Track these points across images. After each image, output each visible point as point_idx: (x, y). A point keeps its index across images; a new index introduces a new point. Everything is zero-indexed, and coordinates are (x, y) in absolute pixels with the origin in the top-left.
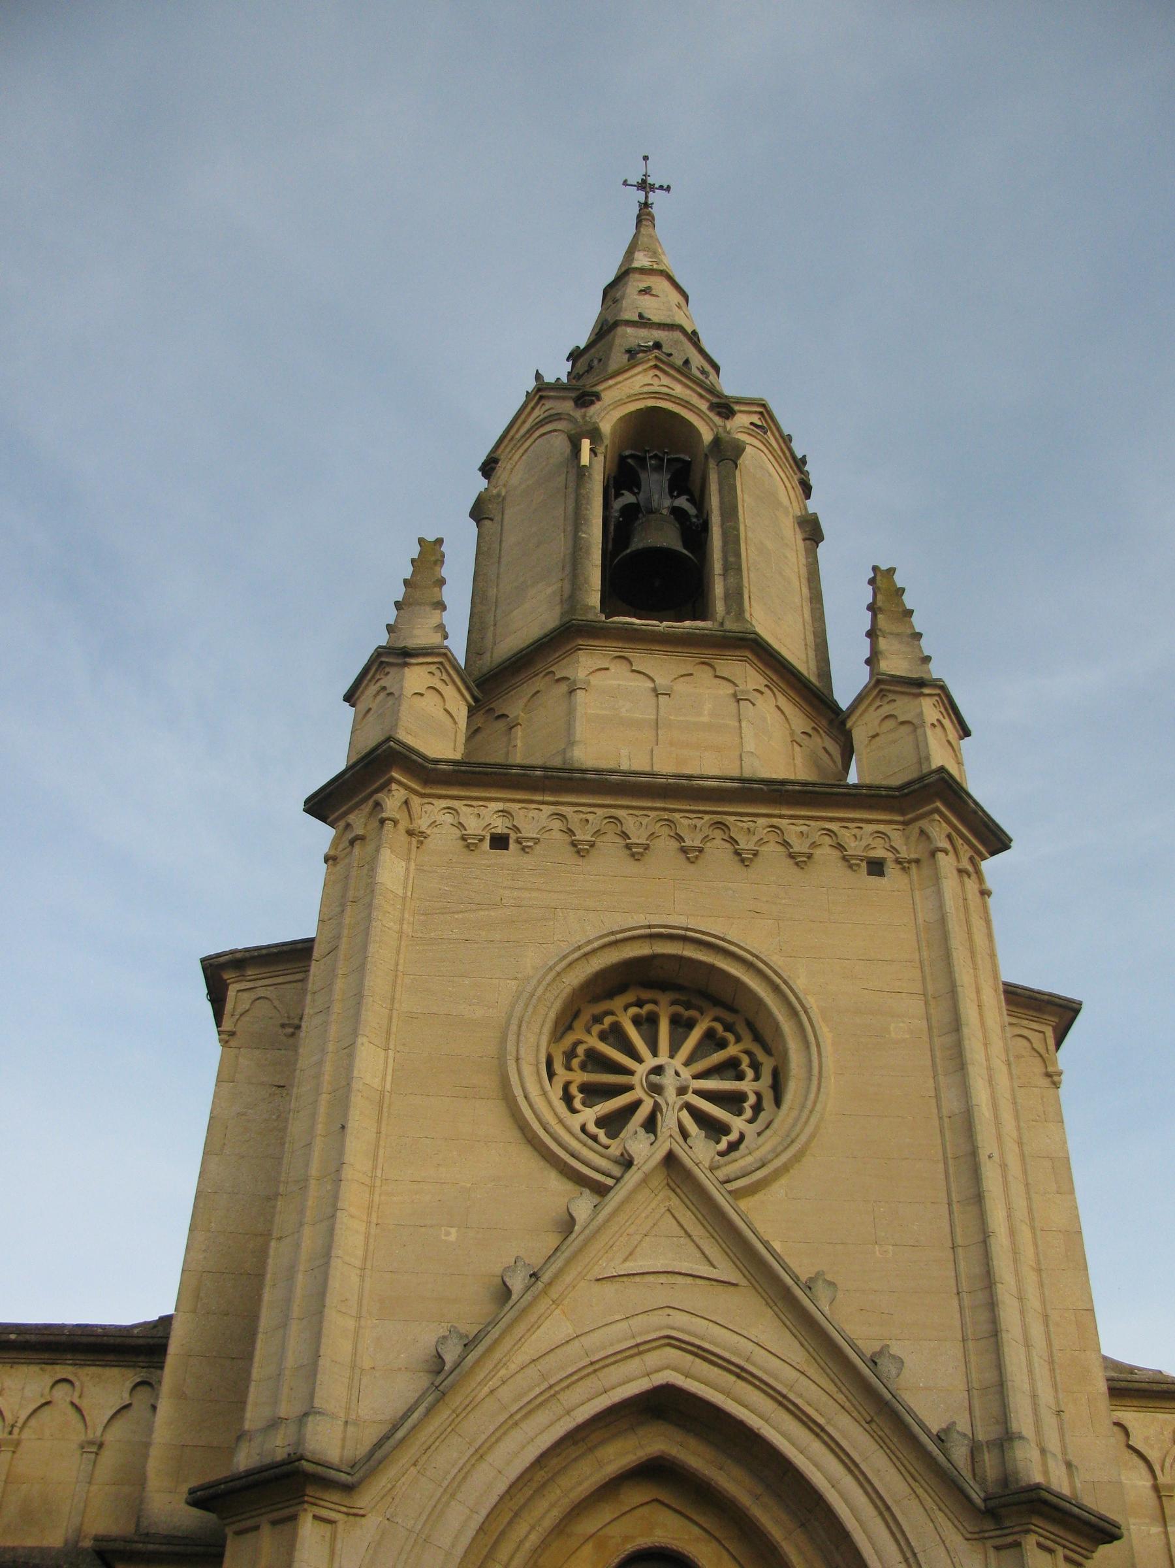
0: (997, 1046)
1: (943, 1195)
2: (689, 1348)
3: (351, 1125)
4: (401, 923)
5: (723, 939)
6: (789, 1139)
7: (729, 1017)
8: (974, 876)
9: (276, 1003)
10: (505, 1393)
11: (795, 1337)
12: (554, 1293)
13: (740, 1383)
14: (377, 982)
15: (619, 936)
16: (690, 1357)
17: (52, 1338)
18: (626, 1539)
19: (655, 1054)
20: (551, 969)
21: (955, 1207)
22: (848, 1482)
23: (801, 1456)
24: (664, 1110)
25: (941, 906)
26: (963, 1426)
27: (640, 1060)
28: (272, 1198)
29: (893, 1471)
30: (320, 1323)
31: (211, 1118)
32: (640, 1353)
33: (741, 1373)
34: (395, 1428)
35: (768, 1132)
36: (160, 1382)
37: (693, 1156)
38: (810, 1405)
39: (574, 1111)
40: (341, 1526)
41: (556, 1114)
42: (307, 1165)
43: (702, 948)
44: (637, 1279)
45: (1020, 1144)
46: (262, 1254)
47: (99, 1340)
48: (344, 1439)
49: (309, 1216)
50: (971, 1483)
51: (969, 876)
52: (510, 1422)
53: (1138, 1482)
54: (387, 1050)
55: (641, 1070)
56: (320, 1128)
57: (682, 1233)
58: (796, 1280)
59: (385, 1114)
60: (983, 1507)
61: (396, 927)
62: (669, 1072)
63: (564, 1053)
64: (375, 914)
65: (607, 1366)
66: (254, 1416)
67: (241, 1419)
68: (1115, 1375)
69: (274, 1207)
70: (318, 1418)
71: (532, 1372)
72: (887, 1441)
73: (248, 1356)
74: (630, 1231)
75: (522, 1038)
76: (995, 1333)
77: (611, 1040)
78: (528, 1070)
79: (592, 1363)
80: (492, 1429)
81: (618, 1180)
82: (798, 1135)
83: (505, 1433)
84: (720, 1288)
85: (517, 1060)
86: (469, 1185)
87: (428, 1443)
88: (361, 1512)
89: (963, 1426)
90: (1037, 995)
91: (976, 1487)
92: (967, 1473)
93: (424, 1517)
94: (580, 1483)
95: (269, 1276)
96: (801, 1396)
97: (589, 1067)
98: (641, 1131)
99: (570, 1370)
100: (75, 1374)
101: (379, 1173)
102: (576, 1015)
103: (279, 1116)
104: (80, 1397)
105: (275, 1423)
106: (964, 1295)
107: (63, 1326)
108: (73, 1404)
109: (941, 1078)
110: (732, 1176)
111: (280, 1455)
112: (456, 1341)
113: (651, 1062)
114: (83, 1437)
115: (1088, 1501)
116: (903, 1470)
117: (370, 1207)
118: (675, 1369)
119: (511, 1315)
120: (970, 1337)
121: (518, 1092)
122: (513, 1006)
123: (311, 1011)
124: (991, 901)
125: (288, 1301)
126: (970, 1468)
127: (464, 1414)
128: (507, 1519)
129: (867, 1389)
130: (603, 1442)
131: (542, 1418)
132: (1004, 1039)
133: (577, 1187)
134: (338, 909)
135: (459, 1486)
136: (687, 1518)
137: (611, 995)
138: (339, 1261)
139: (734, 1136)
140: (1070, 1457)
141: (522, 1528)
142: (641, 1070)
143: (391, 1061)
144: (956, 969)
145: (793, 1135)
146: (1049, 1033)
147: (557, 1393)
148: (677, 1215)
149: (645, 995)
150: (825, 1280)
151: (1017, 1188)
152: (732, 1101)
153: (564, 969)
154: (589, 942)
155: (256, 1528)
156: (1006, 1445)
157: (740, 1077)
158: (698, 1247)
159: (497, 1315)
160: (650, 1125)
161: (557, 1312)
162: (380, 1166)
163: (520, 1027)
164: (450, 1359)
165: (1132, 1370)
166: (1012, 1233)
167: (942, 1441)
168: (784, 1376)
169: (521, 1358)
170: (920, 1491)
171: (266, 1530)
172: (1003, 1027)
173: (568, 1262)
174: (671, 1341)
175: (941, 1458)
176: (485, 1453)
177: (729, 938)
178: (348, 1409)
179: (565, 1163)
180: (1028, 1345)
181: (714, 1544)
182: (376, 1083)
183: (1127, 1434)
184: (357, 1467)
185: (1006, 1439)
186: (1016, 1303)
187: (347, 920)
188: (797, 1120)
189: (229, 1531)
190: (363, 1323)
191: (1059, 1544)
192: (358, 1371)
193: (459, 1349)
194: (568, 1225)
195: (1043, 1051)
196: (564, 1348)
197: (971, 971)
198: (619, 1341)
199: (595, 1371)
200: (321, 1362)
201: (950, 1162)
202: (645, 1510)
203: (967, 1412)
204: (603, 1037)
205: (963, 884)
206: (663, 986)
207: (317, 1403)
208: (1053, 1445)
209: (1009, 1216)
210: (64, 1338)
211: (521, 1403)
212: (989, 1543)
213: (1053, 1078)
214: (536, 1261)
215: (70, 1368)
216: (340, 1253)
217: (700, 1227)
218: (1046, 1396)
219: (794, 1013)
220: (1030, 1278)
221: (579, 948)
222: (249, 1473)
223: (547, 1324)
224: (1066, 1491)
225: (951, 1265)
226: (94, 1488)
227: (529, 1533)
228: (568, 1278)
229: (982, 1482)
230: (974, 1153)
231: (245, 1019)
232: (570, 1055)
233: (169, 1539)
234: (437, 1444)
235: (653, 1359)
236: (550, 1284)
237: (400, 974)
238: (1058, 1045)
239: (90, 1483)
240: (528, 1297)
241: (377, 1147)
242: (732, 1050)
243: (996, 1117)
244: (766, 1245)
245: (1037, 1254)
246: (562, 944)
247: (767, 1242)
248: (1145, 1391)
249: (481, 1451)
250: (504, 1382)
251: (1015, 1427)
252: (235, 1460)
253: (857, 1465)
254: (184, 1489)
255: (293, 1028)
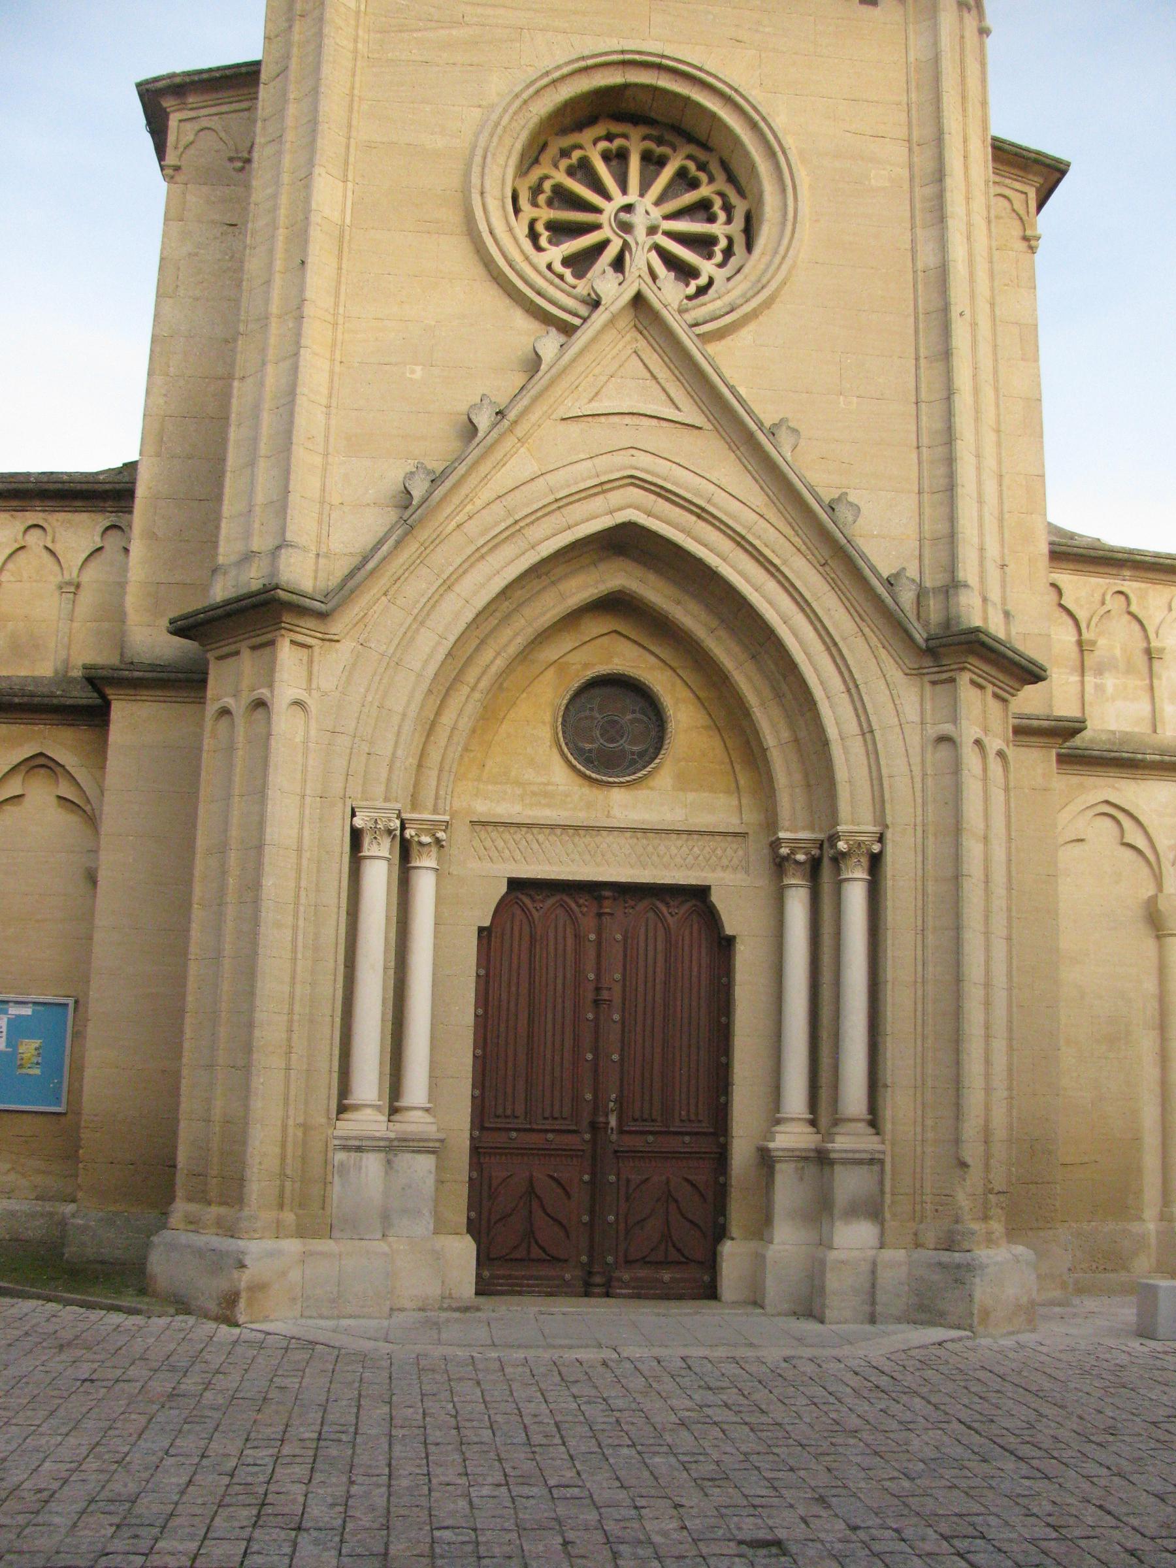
0: (978, 204)
1: (911, 350)
2: (653, 488)
3: (311, 260)
4: (356, 41)
5: (700, 69)
6: (760, 285)
7: (702, 155)
8: (974, 12)
9: (222, 134)
10: (472, 527)
11: (757, 481)
12: (520, 431)
13: (701, 524)
14: (332, 107)
15: (590, 62)
16: (653, 497)
17: (20, 486)
18: (586, 666)
19: (624, 191)
20: (517, 96)
21: (922, 362)
22: (800, 620)
23: (756, 594)
24: (634, 249)
25: (936, 43)
26: (912, 572)
27: (608, 197)
28: (230, 341)
29: (842, 610)
30: (288, 460)
31: (162, 259)
32: (604, 492)
33: (701, 513)
34: (365, 560)
35: (739, 277)
36: (130, 527)
37: (662, 299)
38: (767, 546)
39: (539, 249)
40: (317, 650)
41: (522, 252)
42: (267, 301)
43: (677, 78)
44: (603, 419)
45: (992, 305)
46: (224, 398)
47: (67, 486)
48: (316, 571)
49: (271, 354)
50: (916, 624)
51: (969, 10)
52: (477, 555)
53: (1065, 636)
54: (345, 181)
55: (610, 208)
56: (278, 265)
57: (648, 375)
58: (760, 425)
59: (346, 249)
60: (923, 645)
61: (351, 46)
62: (640, 210)
63: (530, 188)
64: (326, 31)
65: (571, 503)
66: (227, 550)
67: (214, 556)
68: (1057, 540)
69: (233, 350)
70: (290, 550)
71: (497, 507)
72: (839, 583)
73: (218, 497)
74: (596, 371)
75: (487, 170)
76: (950, 488)
77: (579, 175)
78: (493, 205)
79: (557, 500)
80: (459, 561)
81: (585, 320)
82: (768, 282)
83: (471, 566)
84: (685, 431)
85: (482, 193)
86: (433, 323)
87: (398, 574)
88: (336, 638)
89: (912, 572)
90: (1024, 153)
91: (919, 628)
92: (912, 616)
93: (396, 642)
94: (544, 614)
95: (233, 416)
96: (759, 537)
97: (556, 204)
98: (610, 270)
99: (535, 507)
100: (46, 520)
101: (341, 310)
102: (544, 147)
103: (232, 257)
104: (53, 541)
105: (248, 557)
106: (924, 450)
107: (29, 474)
108: (47, 548)
109: (918, 231)
110: (701, 320)
111: (255, 586)
112: (423, 476)
113: (620, 200)
114: (60, 578)
115: (1020, 647)
116: (852, 611)
117: (334, 345)
118: (637, 508)
119: (477, 453)
120: (926, 489)
121: (483, 227)
122: (477, 135)
123: (263, 140)
124: (989, 41)
125: (255, 440)
126: (915, 612)
127: (432, 547)
128: (474, 646)
129: (824, 535)
130: (566, 576)
131: (508, 551)
132: (987, 193)
133: (543, 326)
134: (286, 25)
135: (428, 614)
136: (644, 648)
137: (579, 126)
138: (305, 398)
139: (703, 281)
140: (1008, 607)
141: (488, 654)
142: (610, 208)
143: (350, 194)
144: (946, 113)
145: (764, 281)
146: (1032, 194)
147: (522, 528)
148: (643, 357)
149: (616, 128)
150: (789, 427)
151: (984, 349)
152: (703, 244)
153: (531, 97)
154: (558, 67)
155: (237, 653)
156: (951, 592)
157: (712, 219)
158: (664, 390)
159: (463, 452)
160: (618, 264)
161: (523, 450)
162: (342, 303)
163: (485, 158)
164: (417, 493)
165: (1072, 536)
166: (976, 391)
167: (892, 585)
168: (743, 518)
169: (486, 494)
170: (866, 630)
171: (246, 654)
172: (987, 182)
173: (535, 400)
174: (635, 481)
175: (889, 600)
176: (453, 584)
177: (706, 67)
178: (319, 542)
179: (532, 301)
180: (980, 502)
181: (670, 673)
182: (336, 217)
183: (1059, 592)
184: (329, 597)
185: (952, 586)
186: (973, 460)
187: (296, 37)
188: (771, 262)
189: (210, 656)
190: (330, 459)
191: (990, 682)
192: (327, 507)
193: (427, 484)
194: (534, 363)
195: (1022, 212)
196: (529, 485)
197: (961, 118)
198: (584, 480)
199: (559, 508)
200: (291, 497)
201: (921, 316)
202: (605, 639)
203: (917, 561)
204: (571, 172)
205: (961, 19)
206: (636, 119)
207: (289, 536)
208: (995, 595)
209: (975, 376)
210: (31, 486)
211: (488, 537)
212: (927, 678)
213: (1030, 242)
214: (502, 400)
215: (41, 515)
216: (305, 391)
217: (666, 369)
218: (993, 550)
219: (772, 155)
220: (989, 438)
221: (547, 73)
222: (227, 603)
223: (513, 461)
224: (1001, 635)
225: (913, 421)
226: (75, 624)
227: (495, 658)
228: (533, 417)
229: (926, 625)
230: (945, 309)
231: (192, 151)
232: (536, 190)
233: (153, 667)
234: (406, 575)
235: (616, 497)
236: (515, 422)
237: (356, 99)
238: (1040, 206)
239: (72, 620)
240: (494, 434)
241: (339, 282)
242: (705, 191)
243: (971, 274)
244: (732, 389)
245: (998, 415)
246: (529, 69)
247: (733, 387)
248: (1082, 556)
249: (448, 583)
250: (470, 518)
251: (961, 575)
252: (212, 592)
253: (809, 605)
254: (165, 622)
255: (244, 162)
